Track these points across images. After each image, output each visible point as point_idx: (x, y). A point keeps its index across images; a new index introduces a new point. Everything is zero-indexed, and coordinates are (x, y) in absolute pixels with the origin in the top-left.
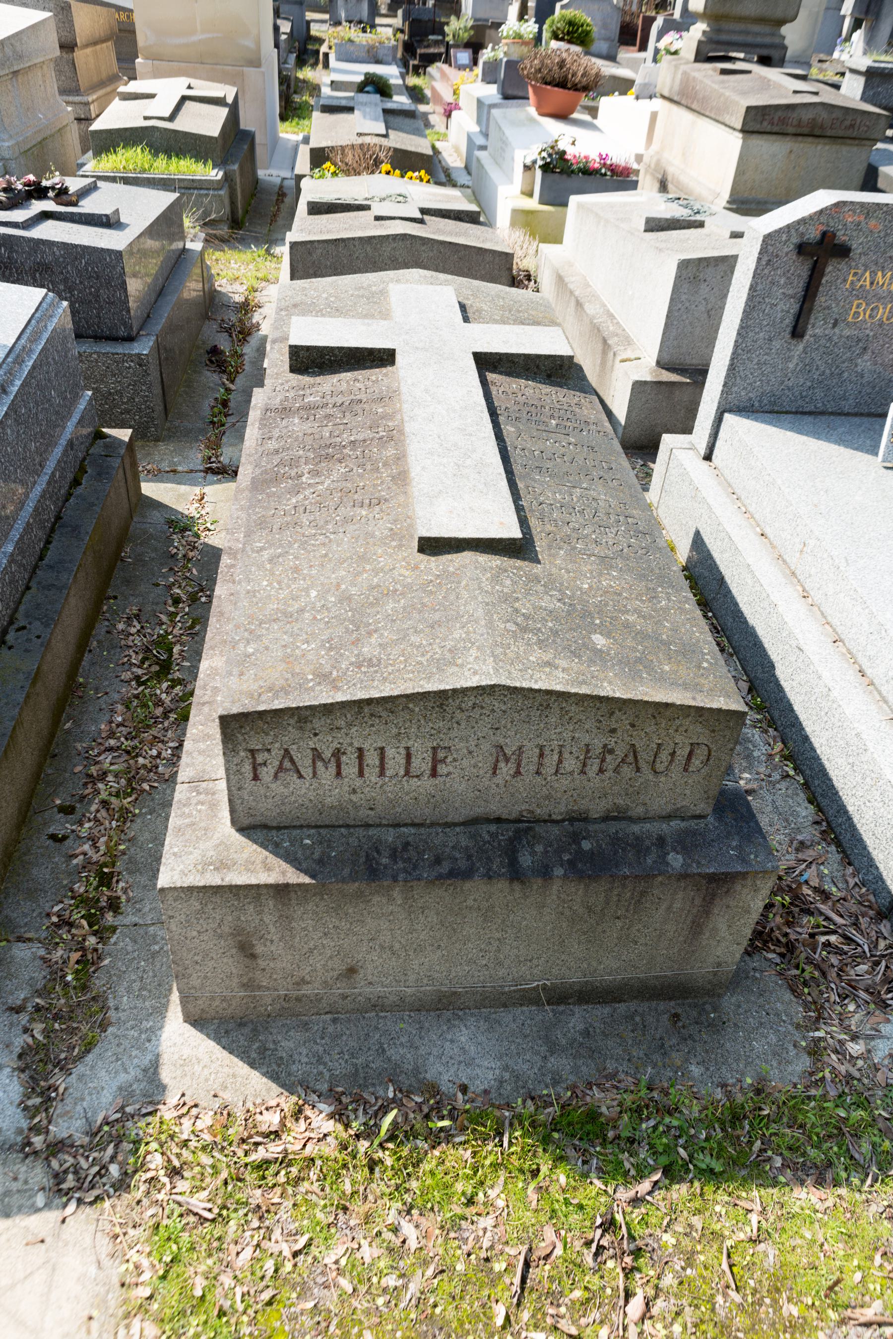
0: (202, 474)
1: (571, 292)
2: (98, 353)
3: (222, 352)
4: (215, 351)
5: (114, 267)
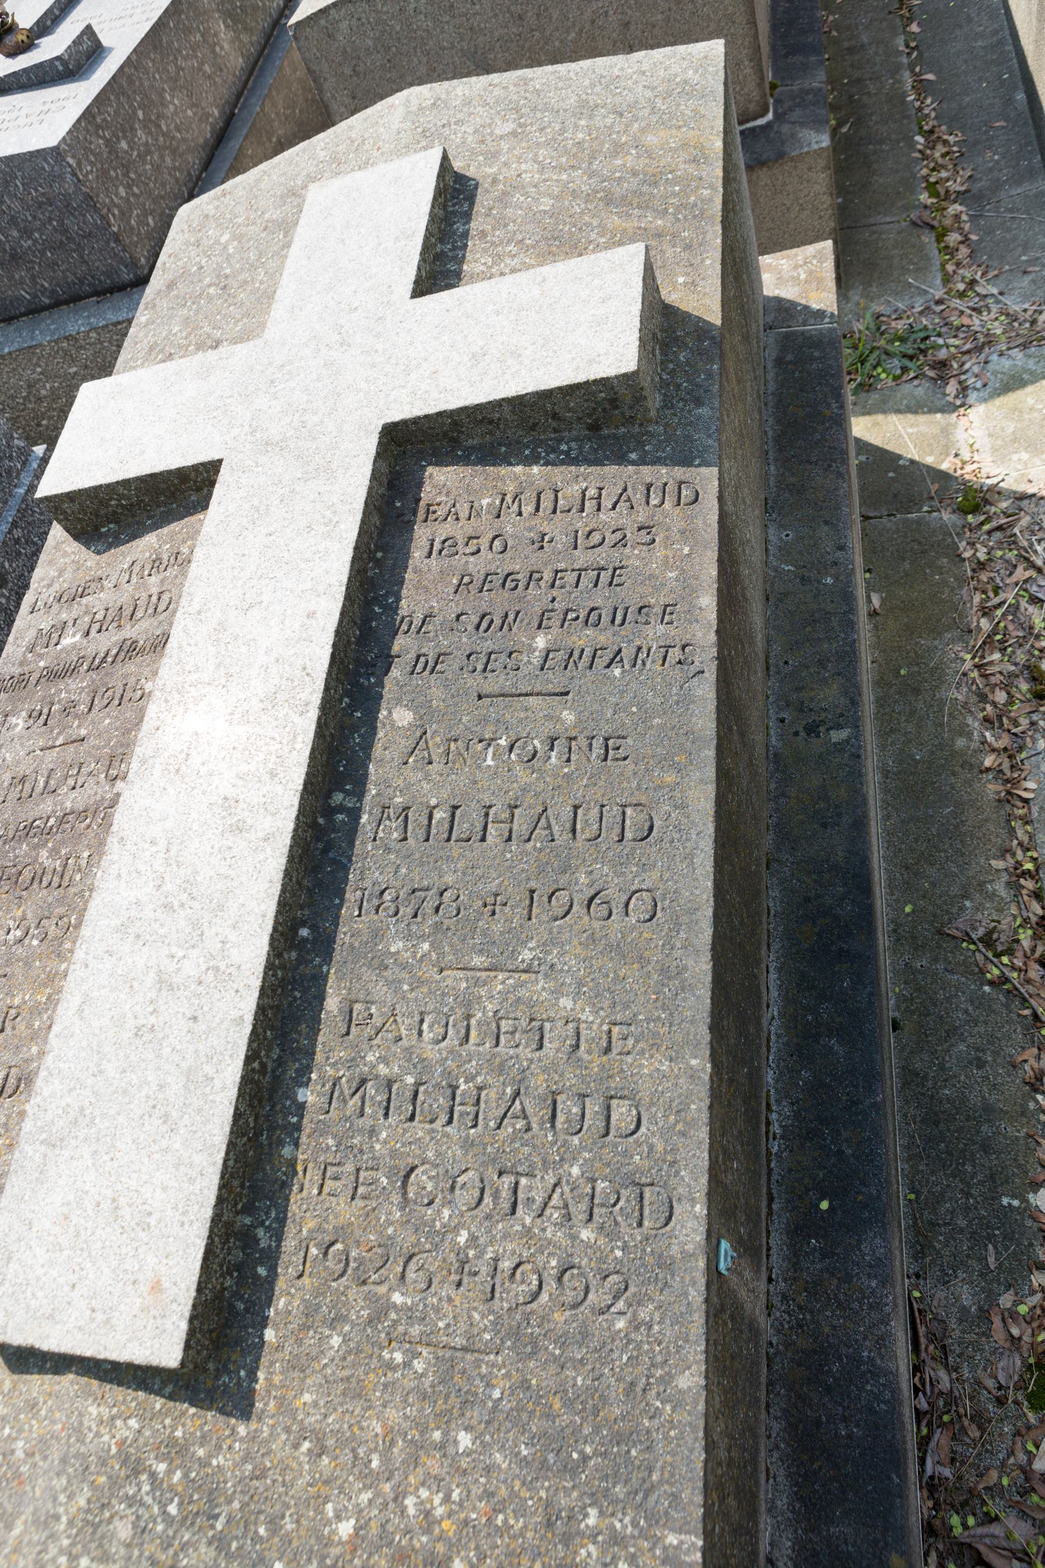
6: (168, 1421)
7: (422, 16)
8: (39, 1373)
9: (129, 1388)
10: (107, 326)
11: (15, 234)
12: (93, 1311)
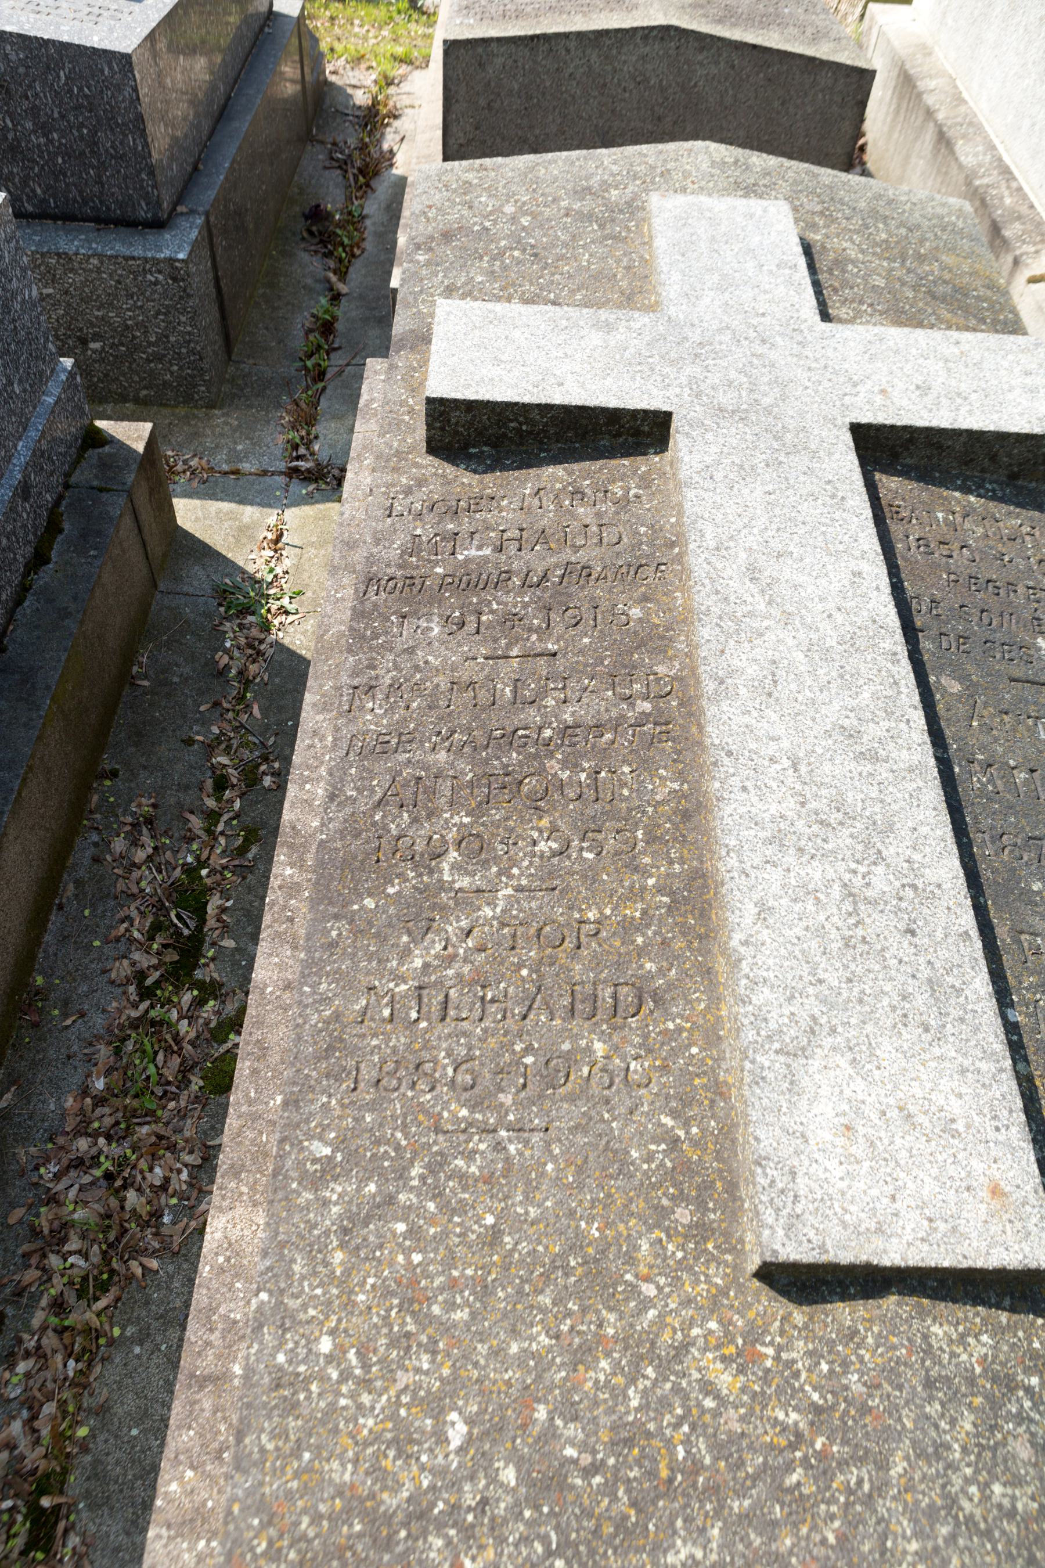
0: (281, 480)
1: (929, 113)
2: (100, 256)
3: (329, 216)
4: (316, 215)
5: (119, 88)
6: (1021, 1334)
7: (574, 83)
8: (843, 1300)
9: (965, 1304)
10: (117, 257)
11: (29, 125)
12: (931, 1220)
